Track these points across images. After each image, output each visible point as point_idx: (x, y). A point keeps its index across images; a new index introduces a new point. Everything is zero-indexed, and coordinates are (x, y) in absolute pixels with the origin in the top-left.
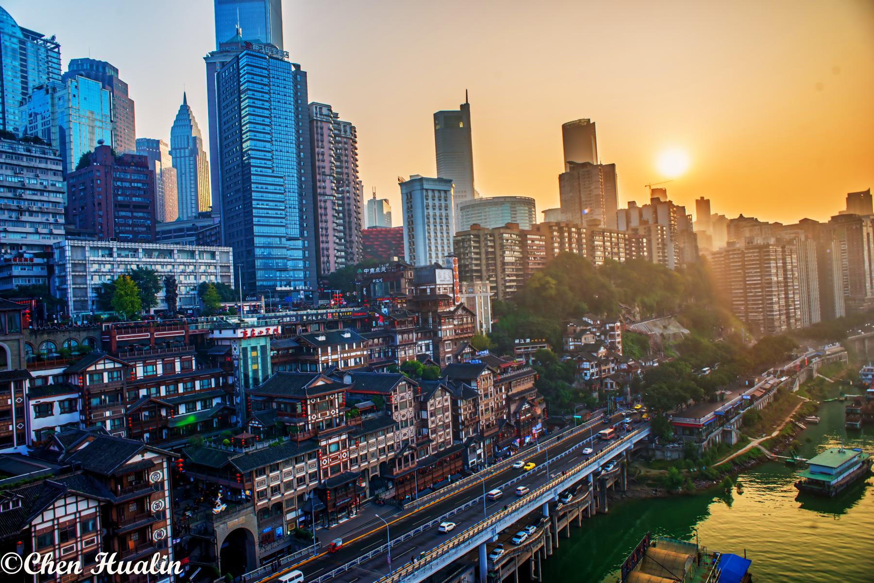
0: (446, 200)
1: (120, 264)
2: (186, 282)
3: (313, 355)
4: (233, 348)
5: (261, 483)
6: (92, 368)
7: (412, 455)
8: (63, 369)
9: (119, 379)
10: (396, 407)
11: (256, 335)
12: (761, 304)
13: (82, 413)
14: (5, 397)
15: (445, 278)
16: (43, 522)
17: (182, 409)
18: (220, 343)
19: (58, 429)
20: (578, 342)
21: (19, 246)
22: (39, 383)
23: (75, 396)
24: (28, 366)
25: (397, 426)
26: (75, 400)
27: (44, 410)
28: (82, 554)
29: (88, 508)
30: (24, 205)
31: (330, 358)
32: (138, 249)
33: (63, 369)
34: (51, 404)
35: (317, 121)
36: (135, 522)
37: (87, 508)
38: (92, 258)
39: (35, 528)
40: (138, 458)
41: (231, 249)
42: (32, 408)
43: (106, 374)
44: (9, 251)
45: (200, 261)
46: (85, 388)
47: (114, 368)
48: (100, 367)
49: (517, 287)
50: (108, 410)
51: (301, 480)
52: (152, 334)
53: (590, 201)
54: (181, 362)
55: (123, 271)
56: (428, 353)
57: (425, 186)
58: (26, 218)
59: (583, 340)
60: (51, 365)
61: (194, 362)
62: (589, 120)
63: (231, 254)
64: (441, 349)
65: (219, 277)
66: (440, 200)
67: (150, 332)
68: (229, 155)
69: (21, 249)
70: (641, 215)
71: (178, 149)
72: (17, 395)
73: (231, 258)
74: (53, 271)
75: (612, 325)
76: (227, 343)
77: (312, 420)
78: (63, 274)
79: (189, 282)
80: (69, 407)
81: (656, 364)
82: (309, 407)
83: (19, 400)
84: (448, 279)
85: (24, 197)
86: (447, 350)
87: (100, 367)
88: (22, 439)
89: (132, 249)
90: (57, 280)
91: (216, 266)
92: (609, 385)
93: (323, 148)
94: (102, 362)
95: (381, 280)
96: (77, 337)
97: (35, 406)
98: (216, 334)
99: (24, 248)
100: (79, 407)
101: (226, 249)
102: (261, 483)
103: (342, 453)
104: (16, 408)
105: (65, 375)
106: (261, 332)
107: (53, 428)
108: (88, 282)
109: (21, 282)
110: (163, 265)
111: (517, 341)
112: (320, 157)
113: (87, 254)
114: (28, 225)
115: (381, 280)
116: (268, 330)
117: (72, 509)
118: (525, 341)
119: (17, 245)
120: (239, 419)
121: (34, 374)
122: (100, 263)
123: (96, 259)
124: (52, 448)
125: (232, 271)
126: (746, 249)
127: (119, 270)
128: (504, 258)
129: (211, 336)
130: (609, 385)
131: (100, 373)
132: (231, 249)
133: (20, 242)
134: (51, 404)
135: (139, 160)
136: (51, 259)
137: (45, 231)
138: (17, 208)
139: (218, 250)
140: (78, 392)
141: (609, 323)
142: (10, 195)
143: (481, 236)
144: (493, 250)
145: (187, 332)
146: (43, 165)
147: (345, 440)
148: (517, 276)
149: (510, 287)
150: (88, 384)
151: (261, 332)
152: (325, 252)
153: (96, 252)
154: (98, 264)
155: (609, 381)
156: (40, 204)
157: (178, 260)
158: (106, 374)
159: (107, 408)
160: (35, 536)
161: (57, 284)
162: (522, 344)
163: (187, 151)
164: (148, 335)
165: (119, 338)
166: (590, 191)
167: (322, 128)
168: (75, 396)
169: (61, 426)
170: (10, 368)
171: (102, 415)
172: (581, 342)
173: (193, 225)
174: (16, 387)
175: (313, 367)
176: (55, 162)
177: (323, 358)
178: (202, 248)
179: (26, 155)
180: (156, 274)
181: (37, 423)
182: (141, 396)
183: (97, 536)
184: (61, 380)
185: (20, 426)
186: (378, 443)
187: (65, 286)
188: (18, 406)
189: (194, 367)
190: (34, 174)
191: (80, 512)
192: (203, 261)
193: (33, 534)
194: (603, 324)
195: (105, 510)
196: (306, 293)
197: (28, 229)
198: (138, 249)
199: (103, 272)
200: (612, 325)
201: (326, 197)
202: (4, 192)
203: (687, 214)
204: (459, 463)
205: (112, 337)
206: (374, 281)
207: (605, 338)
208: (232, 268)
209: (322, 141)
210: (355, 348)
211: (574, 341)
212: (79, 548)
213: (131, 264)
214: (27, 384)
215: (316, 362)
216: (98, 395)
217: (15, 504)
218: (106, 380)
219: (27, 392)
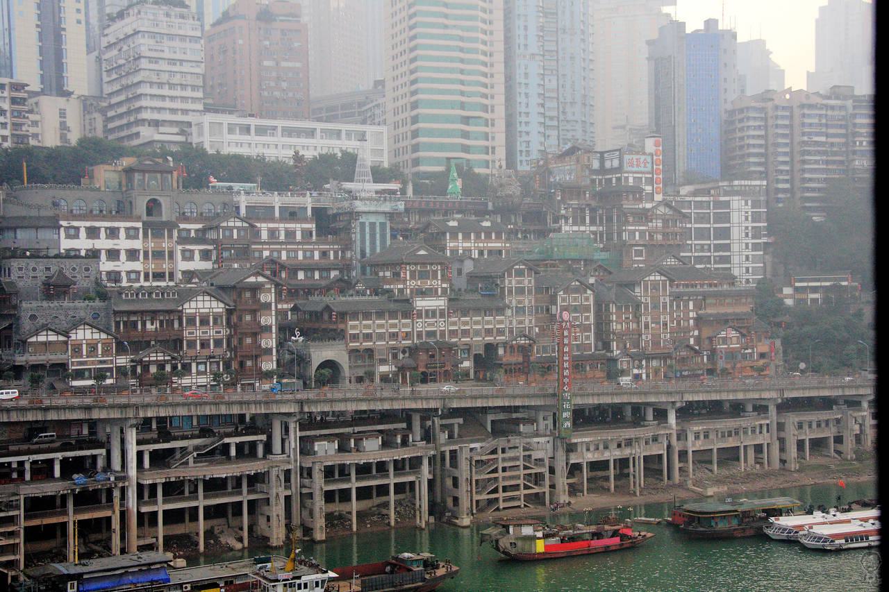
5: (354, 327)
10: (510, 291)
22: (184, 234)
23: (211, 247)
25: (804, 530)
26: (210, 251)
27: (188, 256)
31: (460, 245)
34: (118, 229)
37: (218, 307)
42: (179, 252)
48: (231, 224)
60: (195, 221)
77: (410, 285)
80: (205, 255)
82: (408, 272)
100: (214, 258)
102: (354, 327)
105: (204, 230)
121: (182, 226)
131: (231, 229)
158: (235, 231)
159: (235, 260)
168: (211, 247)
170: (164, 219)
177: (452, 245)
181: (183, 266)
182: (264, 257)
195: (230, 312)
196: (798, 296)
210: (493, 238)
215: (443, 249)
216: (229, 249)
218: (235, 236)
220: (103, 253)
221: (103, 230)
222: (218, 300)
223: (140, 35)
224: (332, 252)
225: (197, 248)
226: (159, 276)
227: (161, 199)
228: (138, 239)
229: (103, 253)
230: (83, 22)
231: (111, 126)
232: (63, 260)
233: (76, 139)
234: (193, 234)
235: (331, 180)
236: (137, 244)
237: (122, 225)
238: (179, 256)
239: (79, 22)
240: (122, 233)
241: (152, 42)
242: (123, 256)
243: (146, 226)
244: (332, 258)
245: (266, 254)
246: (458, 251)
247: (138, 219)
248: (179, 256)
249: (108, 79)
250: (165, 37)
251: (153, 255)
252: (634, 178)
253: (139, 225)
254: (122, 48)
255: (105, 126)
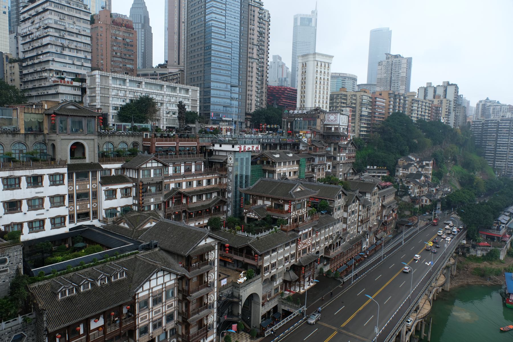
0: (328, 70)
1: (131, 91)
2: (170, 108)
3: (273, 166)
4: (229, 158)
6: (144, 166)
7: (340, 242)
8: (122, 164)
9: (160, 175)
11: (247, 150)
12: (505, 157)
13: (134, 198)
14: (85, 183)
15: (344, 121)
16: (143, 291)
17: (195, 199)
18: (217, 154)
19: (119, 209)
20: (405, 171)
21: (62, 72)
23: (130, 185)
24: (99, 161)
26: (130, 188)
27: (111, 195)
28: (165, 315)
29: (171, 280)
30: (66, 43)
32: (142, 82)
33: (122, 164)
34: (41, 176)
35: (251, 5)
36: (198, 291)
37: (170, 280)
38: (113, 86)
39: (138, 296)
40: (203, 243)
41: (199, 88)
42: (103, 192)
43: (152, 171)
44: (55, 75)
45: (180, 95)
46: (139, 180)
47: (158, 166)
48: (149, 165)
49: (367, 131)
50: (152, 197)
51: (286, 259)
52: (178, 143)
53: (398, 80)
54: (185, 166)
55: (132, 96)
56: (329, 171)
57: (317, 59)
58: (66, 52)
59: (410, 170)
60: (114, 161)
61: (203, 166)
62: (389, 28)
63: (198, 92)
64: (338, 169)
65: (190, 107)
66: (321, 68)
67: (176, 142)
68: (194, 24)
69: (63, 75)
70: (435, 92)
71: (137, 23)
72: (93, 182)
73: (198, 95)
74: (85, 92)
75: (427, 162)
76: (224, 154)
78: (94, 95)
79: (172, 108)
80: (126, 193)
81: (449, 190)
83: (94, 186)
84: (346, 122)
85: (66, 37)
86: (340, 170)
87: (149, 165)
88: (95, 214)
89: (139, 81)
90: (88, 98)
91: (189, 99)
92: (424, 201)
93: (253, 25)
94: (151, 162)
95: (302, 119)
96: (127, 141)
97: (105, 191)
98: (217, 147)
99: (65, 74)
100: (133, 193)
101: (195, 88)
103: (308, 240)
104: (92, 191)
105: (123, 169)
106: (249, 148)
107: (116, 208)
108: (110, 102)
109: (64, 98)
110: (157, 94)
111: (368, 167)
112: (252, 31)
113: (110, 82)
114: (67, 57)
115: (302, 119)
116: (253, 147)
117: (160, 281)
118: (373, 167)
119: (60, 71)
120: (229, 209)
121: (104, 166)
122: (118, 89)
123: (115, 86)
124: (122, 225)
125: (198, 103)
126: (501, 120)
127: (130, 96)
128: (361, 112)
129: (212, 148)
130: (424, 201)
131: (149, 169)
132: (199, 88)
133: (63, 70)
134: (41, 176)
135: (127, 23)
136: (84, 83)
137: (79, 63)
138: (61, 45)
139: (191, 88)
140: (133, 183)
141: (425, 161)
142: (57, 35)
143: (348, 96)
144: (355, 106)
145: (198, 143)
146: (78, 15)
147: (311, 231)
148: (368, 124)
149: (362, 131)
150: (141, 178)
151: (249, 148)
152: (250, 98)
153: (115, 81)
154: (117, 90)
155: (424, 198)
156: (75, 43)
157: (167, 93)
158: (152, 171)
160: (138, 302)
161: (88, 102)
162: (372, 170)
163: (140, 24)
164: (174, 144)
165: (157, 144)
166: (398, 73)
167: (254, 11)
168: (130, 185)
169: (121, 207)
170: (87, 161)
171: (149, 201)
172: (408, 171)
173: (155, 72)
174: (92, 176)
175: (271, 175)
176: (86, 13)
178: (181, 86)
179: (68, 7)
180: (154, 101)
181: (106, 204)
182: (171, 188)
183: (175, 301)
184: (119, 173)
185: (95, 205)
186: (325, 234)
187: (94, 104)
188: (94, 190)
189: (203, 170)
190: (72, 21)
191: (165, 283)
192: (181, 95)
193: (137, 301)
194: (421, 161)
197: (68, 61)
198: (142, 82)
199: (120, 96)
200: (427, 162)
201: (253, 60)
202: (52, 32)
203: (459, 94)
204: (359, 248)
205: (153, 144)
206: (296, 119)
207: (422, 170)
208: (198, 101)
209: (254, 21)
211: (403, 171)
212: (164, 311)
213: (137, 92)
214: (99, 175)
215: (273, 172)
217: (121, 275)
219: (100, 180)
220: (24, 203)
221: (23, 179)
222: (170, 273)
223: (48, 12)
224: (213, 180)
225: (118, 187)
226: (83, 216)
227: (84, 143)
228: (63, 184)
229: (24, 203)
230: (7, 13)
231: (25, 72)
232: (43, 15)
233: (477, 101)
234: (113, 173)
235: (197, 123)
236: (63, 190)
237: (46, 172)
238: (103, 195)
239: (5, 13)
240: (46, 181)
241: (57, 18)
242: (47, 203)
243: (71, 168)
244: (213, 184)
245: (172, 186)
246: (281, 173)
247: (62, 164)
248: (103, 195)
249: (23, 42)
250: (66, 17)
251: (78, 197)
252: (335, 128)
253: (64, 170)
254: (34, 21)
255: (21, 72)
